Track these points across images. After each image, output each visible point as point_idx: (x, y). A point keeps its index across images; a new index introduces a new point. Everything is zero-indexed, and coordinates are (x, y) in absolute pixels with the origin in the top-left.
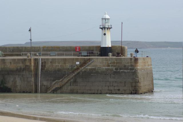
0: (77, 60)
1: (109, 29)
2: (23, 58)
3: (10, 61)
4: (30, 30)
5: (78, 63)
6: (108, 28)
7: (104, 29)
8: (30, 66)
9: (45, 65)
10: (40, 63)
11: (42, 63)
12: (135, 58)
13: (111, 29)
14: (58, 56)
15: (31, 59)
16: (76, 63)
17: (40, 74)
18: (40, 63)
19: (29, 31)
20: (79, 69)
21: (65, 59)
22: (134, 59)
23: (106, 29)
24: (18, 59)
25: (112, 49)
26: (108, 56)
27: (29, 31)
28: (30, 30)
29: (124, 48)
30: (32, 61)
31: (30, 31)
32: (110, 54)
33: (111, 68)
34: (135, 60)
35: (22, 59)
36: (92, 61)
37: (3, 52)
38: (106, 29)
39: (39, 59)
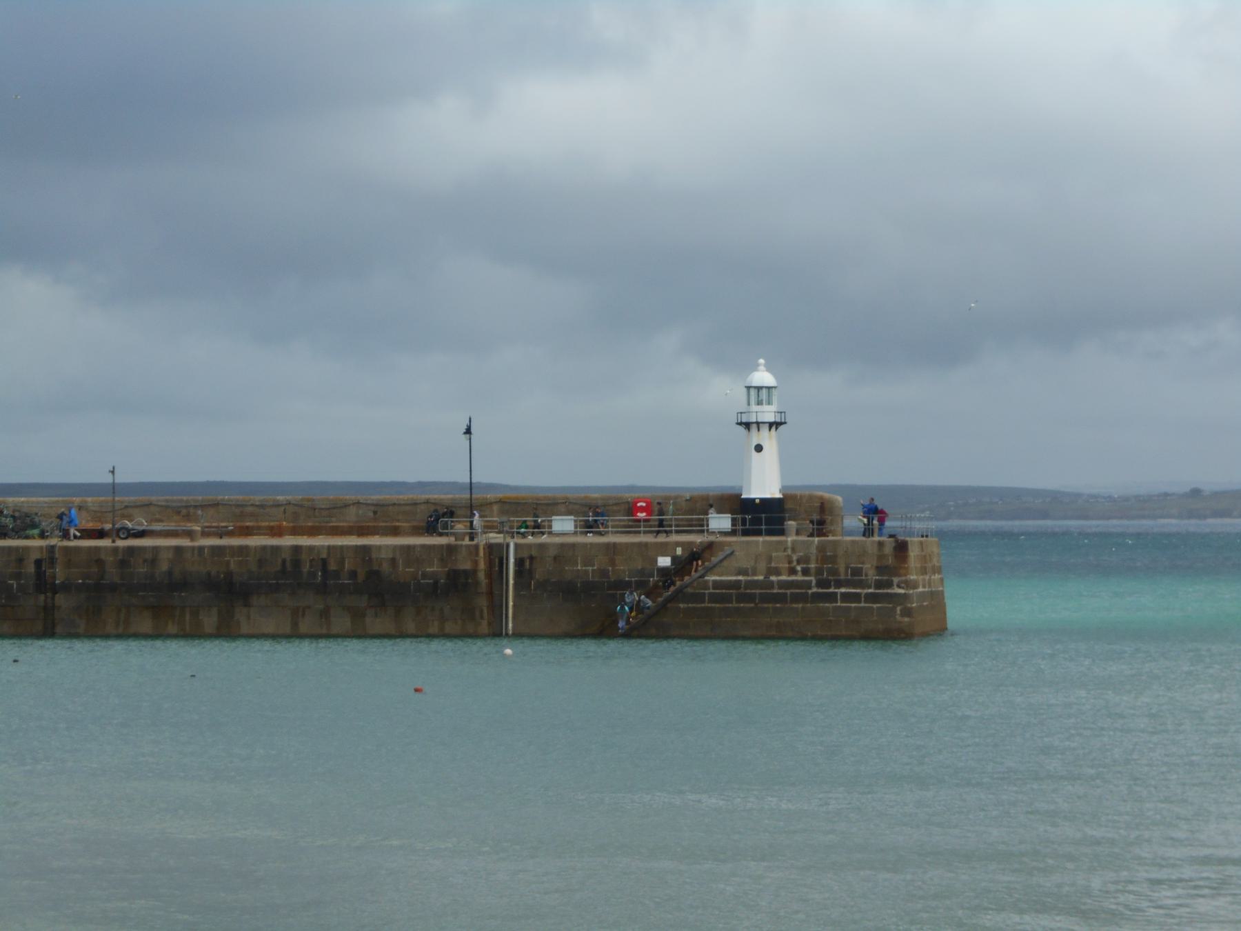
0: (664, 549)
1: (774, 428)
2: (436, 543)
3: (391, 556)
4: (468, 431)
5: (664, 561)
6: (771, 425)
7: (754, 427)
8: (475, 572)
9: (531, 572)
10: (512, 560)
11: (519, 562)
12: (897, 541)
13: (782, 427)
14: (678, 532)
15: (477, 547)
16: (656, 561)
17: (514, 606)
18: (512, 560)
19: (465, 433)
20: (192, 540)
21: (615, 544)
22: (893, 545)
23: (765, 429)
24: (423, 546)
25: (789, 505)
26: (782, 532)
27: (465, 433)
28: (468, 431)
29: (831, 502)
30: (481, 553)
31: (468, 435)
32: (791, 524)
33: (924, 590)
34: (895, 548)
35: (442, 546)
36: (728, 552)
37: (171, 555)
38: (765, 429)
39: (508, 546)
